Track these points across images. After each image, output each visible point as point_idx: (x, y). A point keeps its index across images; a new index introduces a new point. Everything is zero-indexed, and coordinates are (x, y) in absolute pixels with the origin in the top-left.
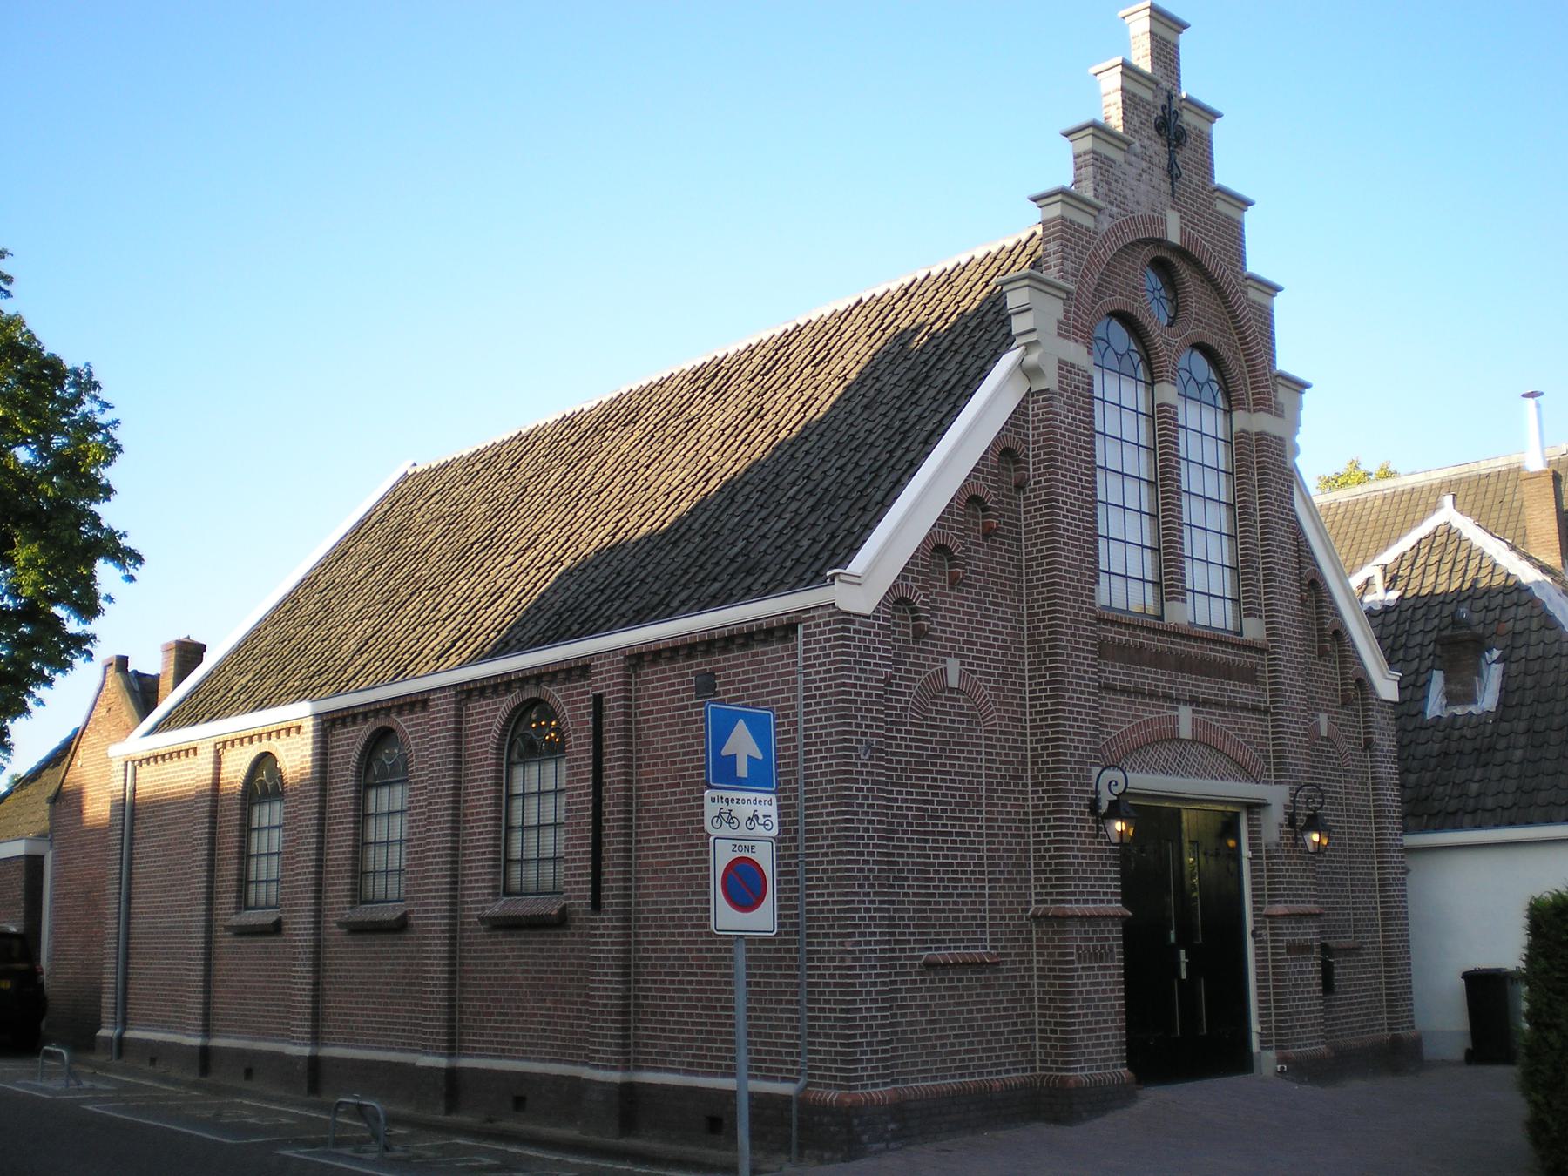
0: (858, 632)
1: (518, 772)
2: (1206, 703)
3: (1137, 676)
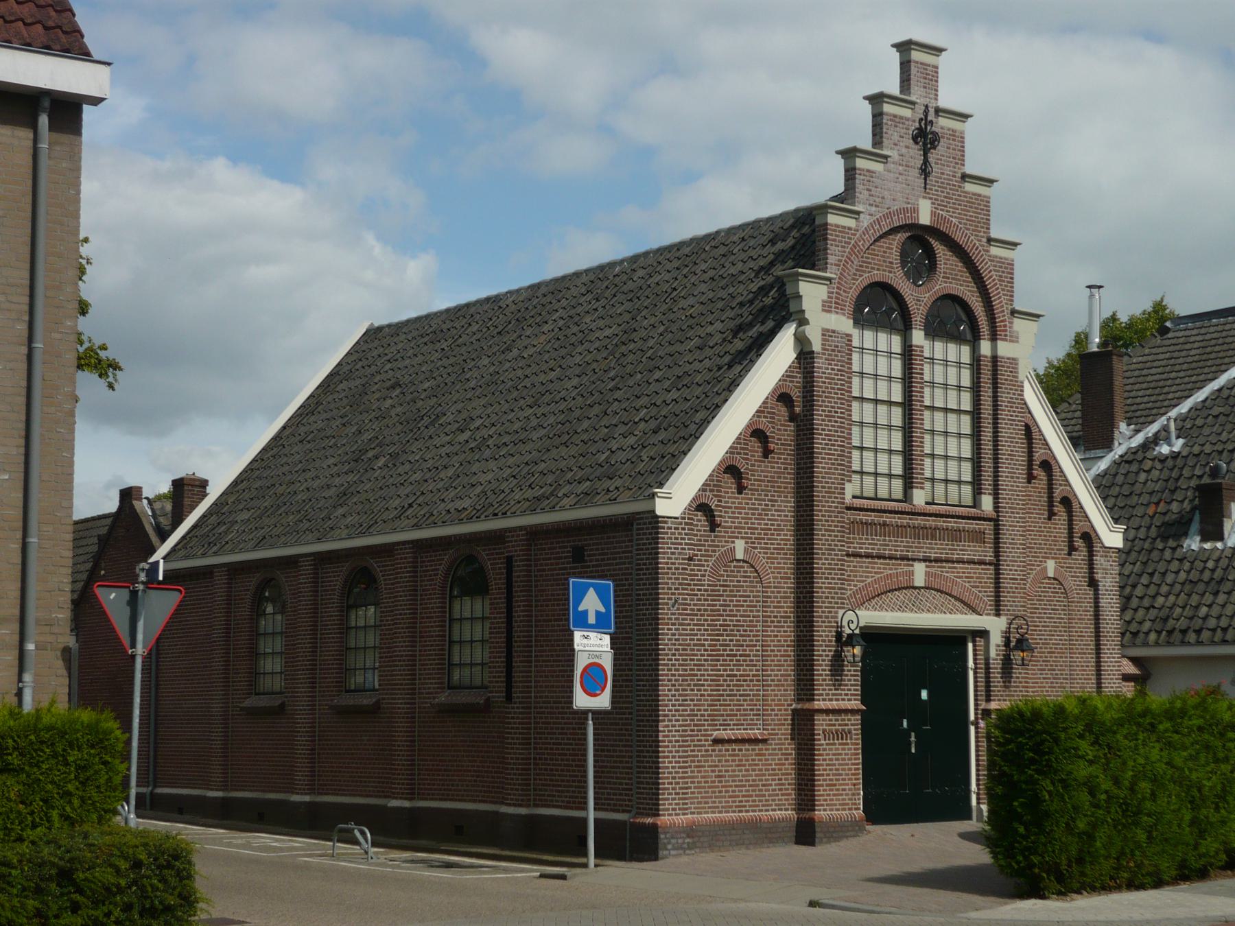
0: (669, 528)
1: (457, 606)
2: (937, 560)
3: (879, 544)
